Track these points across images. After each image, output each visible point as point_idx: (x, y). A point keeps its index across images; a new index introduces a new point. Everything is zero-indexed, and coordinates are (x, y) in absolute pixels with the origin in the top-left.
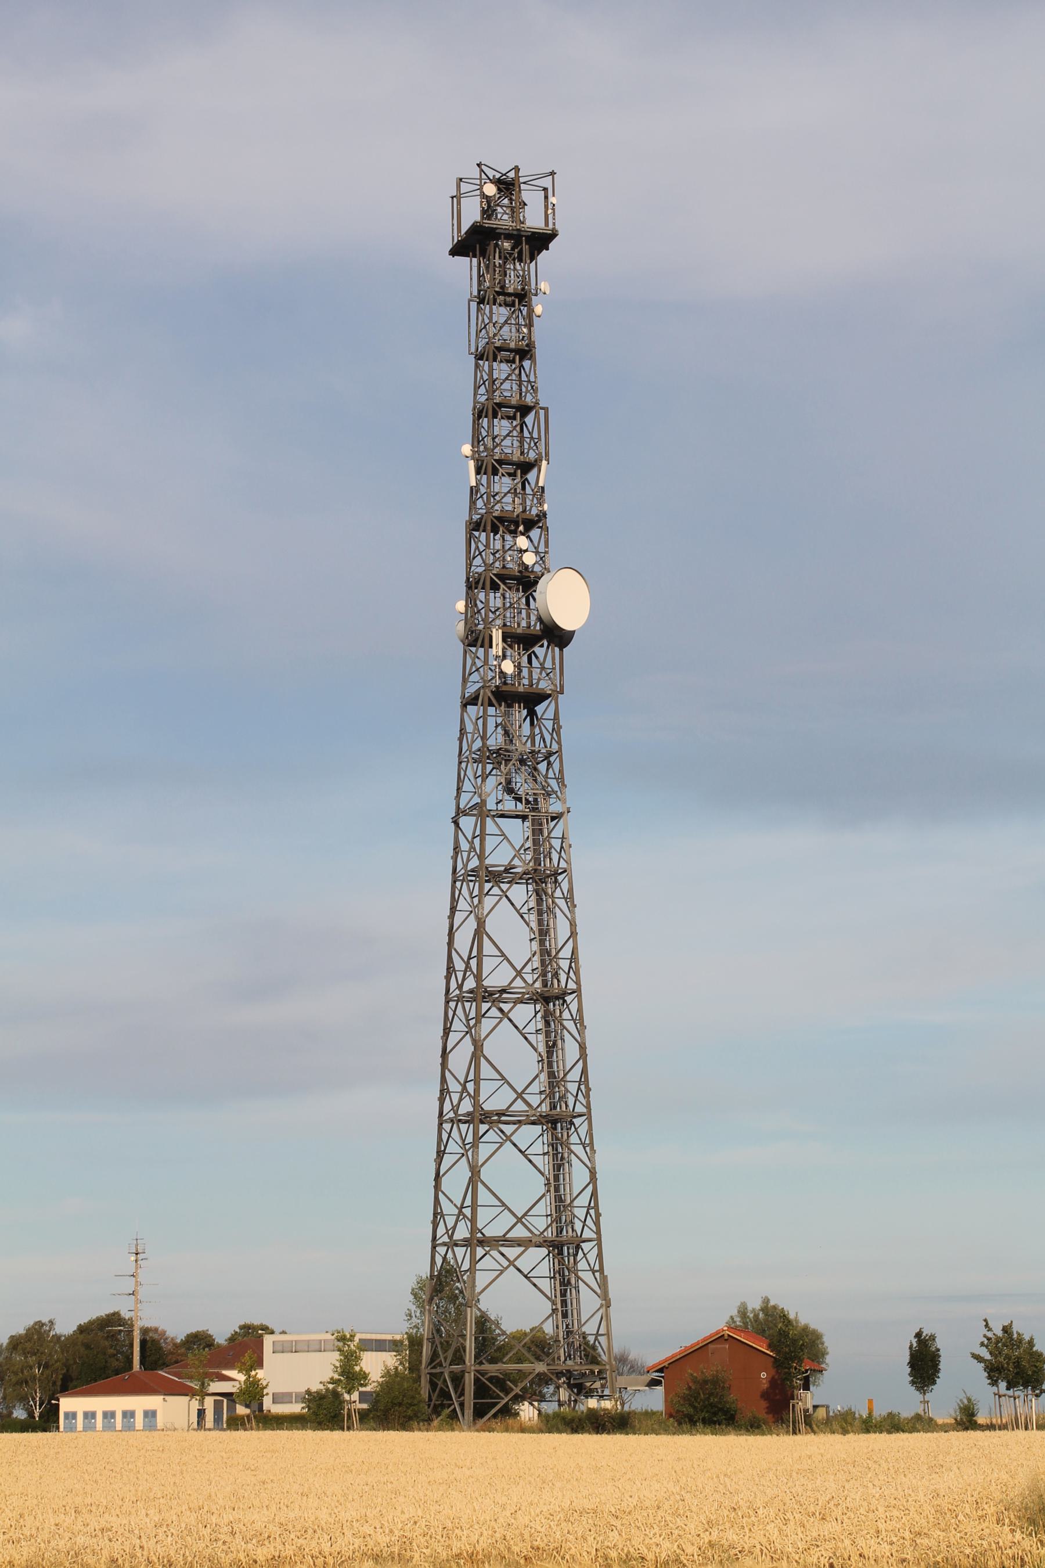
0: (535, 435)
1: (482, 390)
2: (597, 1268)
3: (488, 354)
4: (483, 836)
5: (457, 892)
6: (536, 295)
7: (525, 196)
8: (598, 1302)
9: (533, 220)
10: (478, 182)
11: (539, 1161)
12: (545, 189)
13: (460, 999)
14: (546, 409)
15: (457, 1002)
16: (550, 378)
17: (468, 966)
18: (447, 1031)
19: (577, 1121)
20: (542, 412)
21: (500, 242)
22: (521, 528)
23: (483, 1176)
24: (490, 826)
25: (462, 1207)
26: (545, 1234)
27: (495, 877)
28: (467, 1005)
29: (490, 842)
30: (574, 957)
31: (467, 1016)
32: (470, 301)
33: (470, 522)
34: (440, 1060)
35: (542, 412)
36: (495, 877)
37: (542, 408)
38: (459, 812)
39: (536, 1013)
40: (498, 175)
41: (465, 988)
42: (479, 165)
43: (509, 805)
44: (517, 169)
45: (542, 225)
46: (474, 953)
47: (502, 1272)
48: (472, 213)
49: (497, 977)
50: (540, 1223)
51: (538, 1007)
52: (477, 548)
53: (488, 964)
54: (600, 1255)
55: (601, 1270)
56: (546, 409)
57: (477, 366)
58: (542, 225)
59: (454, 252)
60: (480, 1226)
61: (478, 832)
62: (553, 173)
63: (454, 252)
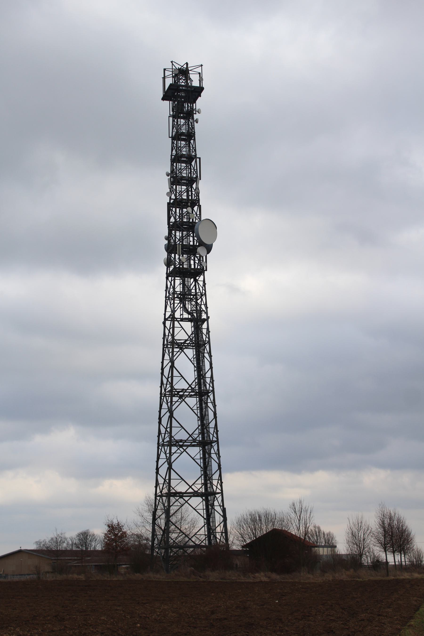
0: (195, 168)
1: (174, 150)
2: (221, 505)
3: (176, 159)
4: (173, 327)
5: (160, 450)
6: (196, 114)
7: (191, 76)
8: (222, 519)
9: (196, 83)
10: (171, 70)
11: (196, 411)
12: (199, 73)
13: (163, 445)
14: (200, 158)
15: (162, 446)
16: (202, 145)
17: (169, 332)
18: (158, 458)
19: (217, 496)
20: (198, 160)
21: (182, 93)
22: (189, 204)
23: (174, 416)
24: (176, 323)
25: (167, 428)
26: (201, 490)
27: (181, 444)
28: (166, 448)
29: (176, 330)
30: (212, 377)
31: (167, 401)
32: (169, 117)
33: (169, 204)
34: (161, 371)
35: (198, 160)
36: (181, 444)
37: (198, 158)
38: (166, 319)
39: (200, 450)
40: (180, 67)
41: (165, 441)
42: (172, 62)
43: (186, 316)
44: (187, 64)
45: (199, 86)
46: (170, 375)
47: (181, 454)
48: (169, 81)
49: (180, 385)
50: (198, 487)
51: (201, 449)
52: (172, 213)
53: (175, 380)
54: (223, 500)
55: (223, 505)
56: (200, 158)
57: (173, 143)
58: (199, 86)
59: (163, 99)
60: (173, 435)
61: (171, 326)
62: (202, 65)
63: (163, 99)
